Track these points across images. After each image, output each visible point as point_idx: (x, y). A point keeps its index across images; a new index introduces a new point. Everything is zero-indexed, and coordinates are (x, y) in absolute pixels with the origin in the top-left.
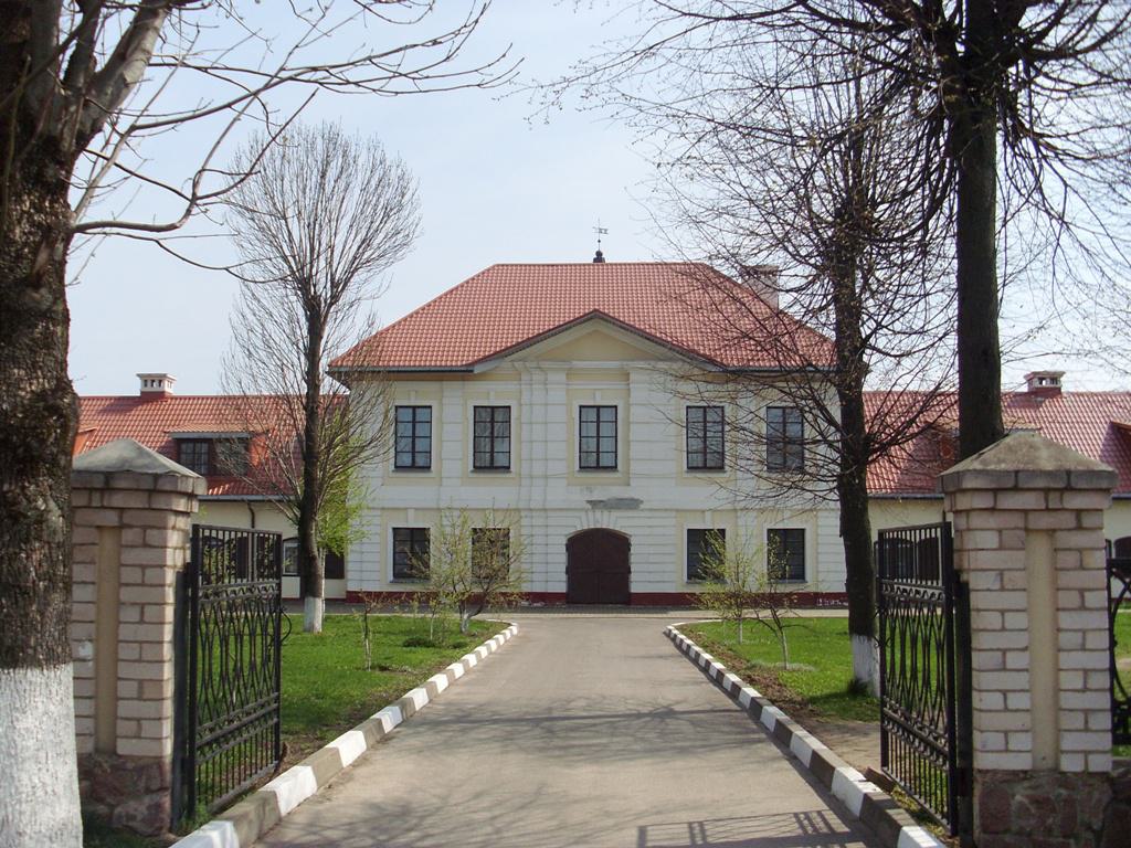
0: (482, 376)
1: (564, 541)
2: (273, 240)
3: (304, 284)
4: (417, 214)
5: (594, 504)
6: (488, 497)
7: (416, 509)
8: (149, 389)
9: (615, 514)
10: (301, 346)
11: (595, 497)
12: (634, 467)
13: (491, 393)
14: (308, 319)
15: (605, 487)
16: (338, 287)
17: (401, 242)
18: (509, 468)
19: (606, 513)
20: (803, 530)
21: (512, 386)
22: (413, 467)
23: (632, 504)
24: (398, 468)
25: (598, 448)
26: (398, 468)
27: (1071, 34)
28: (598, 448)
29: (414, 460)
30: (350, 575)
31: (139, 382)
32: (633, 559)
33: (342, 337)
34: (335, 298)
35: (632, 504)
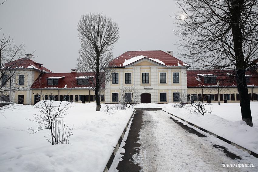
0: (126, 69)
1: (140, 95)
2: (89, 38)
3: (96, 47)
4: (118, 35)
5: (145, 89)
6: (128, 88)
7: (164, 90)
8: (73, 71)
9: (148, 90)
10: (95, 58)
11: (145, 88)
12: (151, 83)
13: (128, 71)
14: (96, 53)
15: (147, 86)
16: (102, 47)
17: (115, 39)
18: (131, 83)
19: (147, 90)
20: (166, 93)
21: (131, 70)
22: (116, 83)
23: (151, 89)
24: (113, 83)
25: (146, 79)
26: (113, 83)
27: (205, 21)
28: (146, 79)
29: (116, 82)
30: (105, 101)
31: (71, 71)
32: (151, 98)
33: (104, 56)
34: (101, 50)
35: (151, 89)
